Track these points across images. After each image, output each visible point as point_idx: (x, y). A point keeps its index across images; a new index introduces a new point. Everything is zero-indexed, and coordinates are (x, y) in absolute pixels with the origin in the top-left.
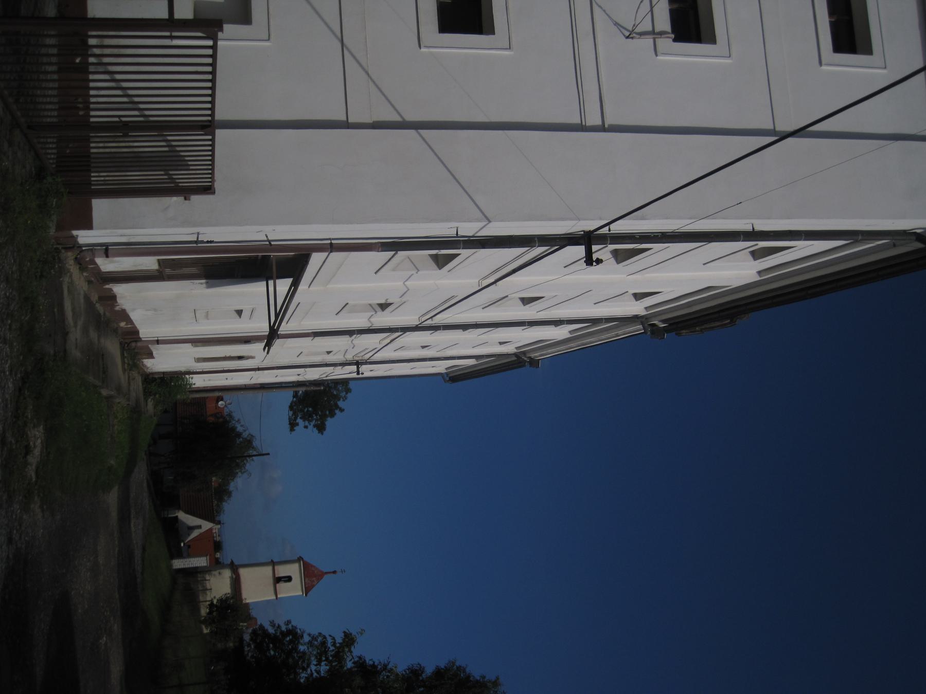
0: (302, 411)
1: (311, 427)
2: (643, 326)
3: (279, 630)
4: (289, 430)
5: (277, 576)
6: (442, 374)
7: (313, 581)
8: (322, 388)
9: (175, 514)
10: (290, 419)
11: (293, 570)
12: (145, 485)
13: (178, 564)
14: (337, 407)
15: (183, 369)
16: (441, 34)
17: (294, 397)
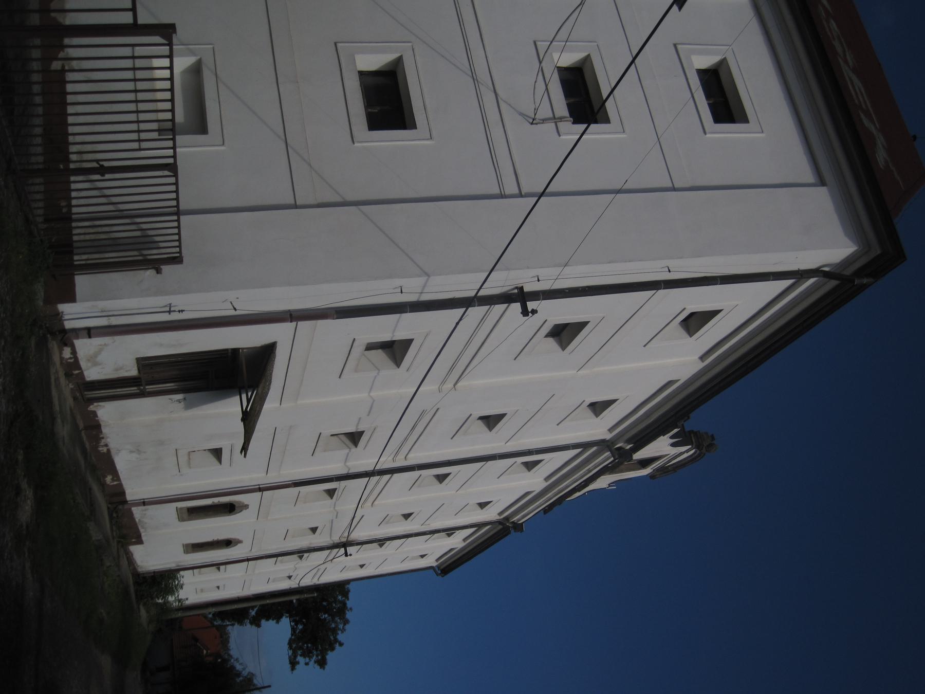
0: (301, 648)
1: (312, 663)
2: (611, 453)
4: (290, 669)
6: (431, 567)
8: (316, 595)
10: (290, 657)
14: (336, 640)
15: (172, 566)
16: (371, 132)
17: (292, 635)
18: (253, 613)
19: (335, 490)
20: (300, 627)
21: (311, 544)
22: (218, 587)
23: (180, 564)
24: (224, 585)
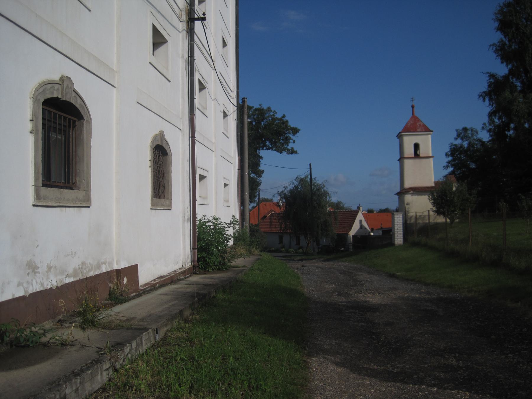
0: (283, 144)
3: (451, 162)
4: (296, 154)
5: (413, 156)
7: (420, 125)
9: (351, 237)
10: (287, 154)
11: (409, 141)
12: (326, 264)
13: (399, 239)
14: (281, 119)
15: (188, 227)
17: (272, 150)
18: (253, 175)
19: (200, 175)
20: (268, 143)
21: (183, 57)
22: (226, 185)
23: (186, 218)
24: (224, 178)
